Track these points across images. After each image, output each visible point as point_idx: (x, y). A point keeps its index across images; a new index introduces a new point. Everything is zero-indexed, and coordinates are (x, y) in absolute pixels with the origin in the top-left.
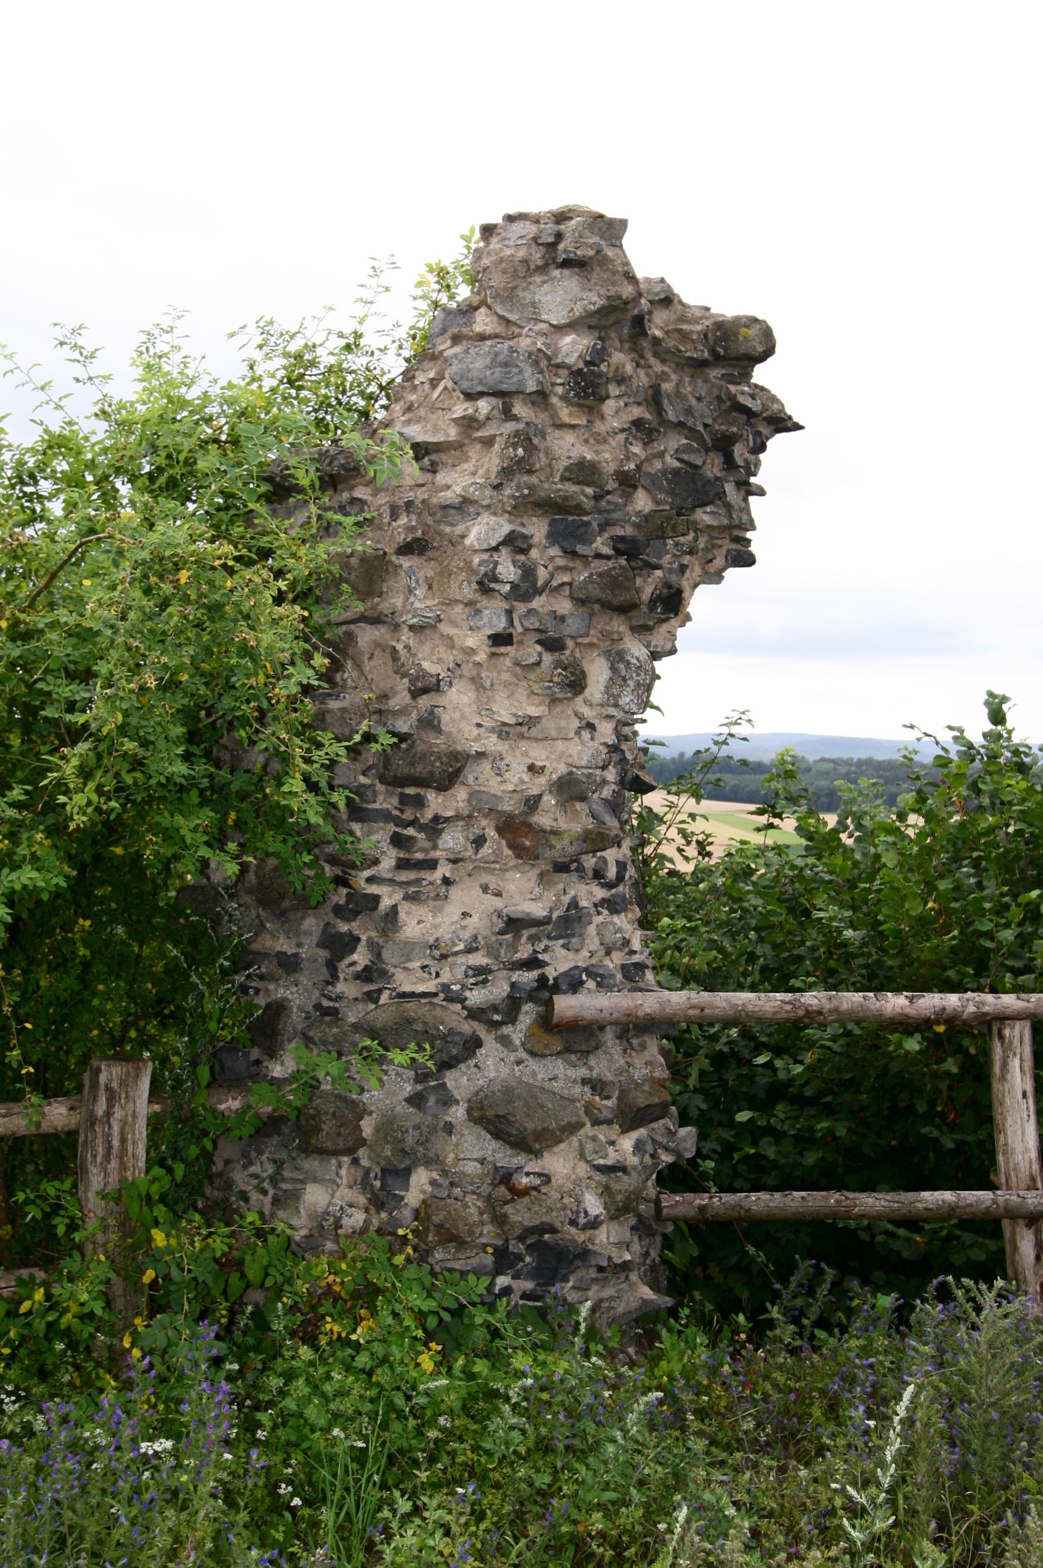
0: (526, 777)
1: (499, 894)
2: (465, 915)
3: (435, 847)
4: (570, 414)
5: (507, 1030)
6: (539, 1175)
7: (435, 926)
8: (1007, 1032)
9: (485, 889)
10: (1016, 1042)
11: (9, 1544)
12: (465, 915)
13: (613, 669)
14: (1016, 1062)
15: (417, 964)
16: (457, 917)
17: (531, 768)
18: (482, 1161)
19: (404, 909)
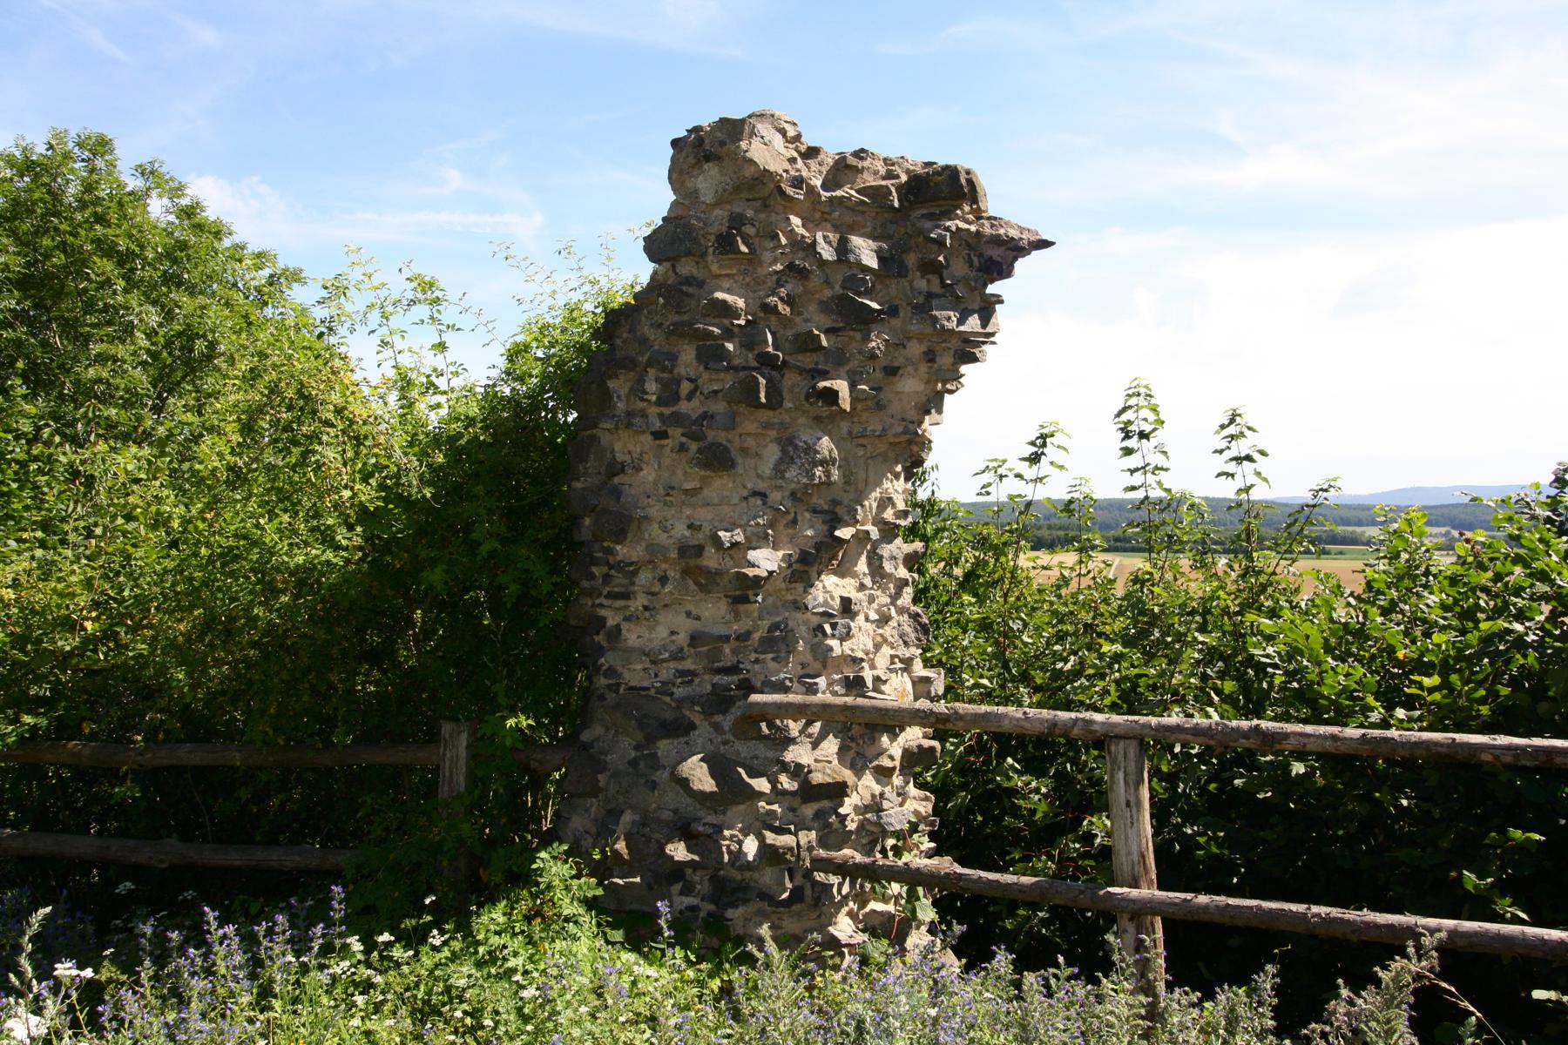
0: (687, 533)
1: (698, 618)
2: (673, 633)
3: (633, 584)
4: (721, 267)
5: (718, 718)
6: (713, 826)
7: (650, 640)
8: (1113, 748)
9: (689, 614)
10: (1120, 757)
11: (460, 1041)
12: (673, 633)
13: (784, 451)
14: (1121, 775)
15: (639, 667)
16: (665, 633)
17: (690, 527)
18: (675, 811)
19: (625, 626)
